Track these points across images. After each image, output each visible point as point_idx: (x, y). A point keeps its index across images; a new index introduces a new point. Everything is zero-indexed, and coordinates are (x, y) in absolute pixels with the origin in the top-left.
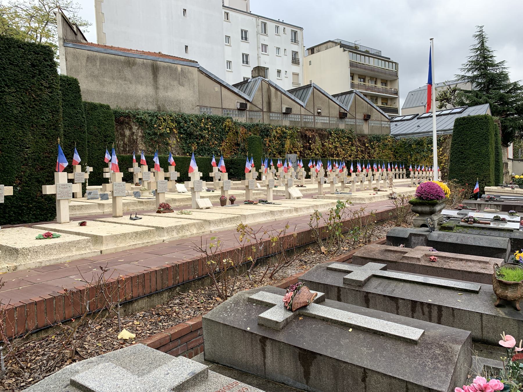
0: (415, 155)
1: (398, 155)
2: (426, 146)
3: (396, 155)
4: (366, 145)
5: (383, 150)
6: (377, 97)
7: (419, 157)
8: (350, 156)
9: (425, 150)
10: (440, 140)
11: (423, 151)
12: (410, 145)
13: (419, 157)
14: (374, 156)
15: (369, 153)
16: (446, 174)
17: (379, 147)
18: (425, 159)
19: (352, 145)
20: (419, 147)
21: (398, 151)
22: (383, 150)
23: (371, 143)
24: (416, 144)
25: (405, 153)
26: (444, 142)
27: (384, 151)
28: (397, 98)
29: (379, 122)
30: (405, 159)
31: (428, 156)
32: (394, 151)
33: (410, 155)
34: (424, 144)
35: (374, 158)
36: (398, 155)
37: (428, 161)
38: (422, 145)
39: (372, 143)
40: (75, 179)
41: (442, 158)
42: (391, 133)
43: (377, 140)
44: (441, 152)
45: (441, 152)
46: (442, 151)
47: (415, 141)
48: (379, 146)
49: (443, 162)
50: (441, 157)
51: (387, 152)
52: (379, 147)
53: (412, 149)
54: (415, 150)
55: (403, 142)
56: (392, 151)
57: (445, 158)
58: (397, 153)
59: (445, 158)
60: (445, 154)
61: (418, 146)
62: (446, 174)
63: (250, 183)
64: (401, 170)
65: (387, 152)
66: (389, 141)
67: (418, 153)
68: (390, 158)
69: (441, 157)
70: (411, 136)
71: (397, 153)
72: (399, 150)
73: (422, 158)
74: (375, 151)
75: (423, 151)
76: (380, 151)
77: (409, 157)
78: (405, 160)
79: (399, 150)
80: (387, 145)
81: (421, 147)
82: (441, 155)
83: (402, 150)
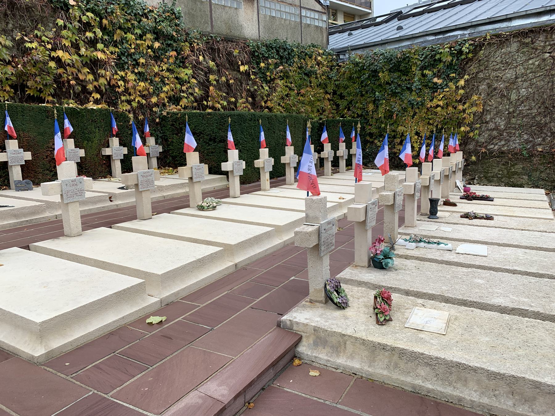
0: (388, 100)
1: (343, 104)
2: (418, 73)
3: (339, 102)
4: (242, 68)
5: (300, 87)
6: (336, 10)
7: (397, 108)
8: (175, 100)
9: (416, 84)
10: (460, 52)
11: (410, 89)
12: (375, 74)
13: (397, 108)
14: (269, 104)
15: (253, 95)
16: (474, 158)
17: (288, 77)
18: (415, 114)
19: (182, 62)
20: (399, 77)
21: (345, 94)
22: (300, 87)
23: (258, 64)
24: (390, 71)
25: (362, 95)
26: (471, 60)
27: (303, 91)
28: (370, 13)
29: (293, 10)
30: (360, 112)
31: (423, 104)
32: (335, 93)
33: (374, 102)
34: (414, 69)
35: (270, 109)
36: (343, 104)
37: (422, 119)
38: (406, 72)
39: (262, 65)
40: (9, 162)
41: (464, 111)
42: (330, 47)
43: (281, 58)
44: (461, 92)
45: (461, 92)
46: (463, 88)
47: (389, 60)
48: (285, 76)
49: (467, 121)
50: (461, 107)
51: (311, 93)
52: (288, 77)
53: (380, 85)
54: (388, 87)
55: (357, 64)
56: (326, 93)
57: (474, 109)
58: (342, 97)
59: (474, 109)
60: (475, 97)
61: (396, 75)
62: (474, 158)
63: (291, 159)
64: (342, 146)
65: (311, 93)
66: (319, 64)
67: (394, 94)
68: (324, 111)
69: (461, 107)
70: (377, 50)
71: (342, 97)
72: (346, 87)
73: (405, 110)
74: (273, 89)
75: (410, 89)
76: (290, 89)
77: (371, 107)
78: (361, 115)
79: (346, 87)
80: (311, 72)
81: (404, 78)
82: (460, 101)
83: (354, 88)
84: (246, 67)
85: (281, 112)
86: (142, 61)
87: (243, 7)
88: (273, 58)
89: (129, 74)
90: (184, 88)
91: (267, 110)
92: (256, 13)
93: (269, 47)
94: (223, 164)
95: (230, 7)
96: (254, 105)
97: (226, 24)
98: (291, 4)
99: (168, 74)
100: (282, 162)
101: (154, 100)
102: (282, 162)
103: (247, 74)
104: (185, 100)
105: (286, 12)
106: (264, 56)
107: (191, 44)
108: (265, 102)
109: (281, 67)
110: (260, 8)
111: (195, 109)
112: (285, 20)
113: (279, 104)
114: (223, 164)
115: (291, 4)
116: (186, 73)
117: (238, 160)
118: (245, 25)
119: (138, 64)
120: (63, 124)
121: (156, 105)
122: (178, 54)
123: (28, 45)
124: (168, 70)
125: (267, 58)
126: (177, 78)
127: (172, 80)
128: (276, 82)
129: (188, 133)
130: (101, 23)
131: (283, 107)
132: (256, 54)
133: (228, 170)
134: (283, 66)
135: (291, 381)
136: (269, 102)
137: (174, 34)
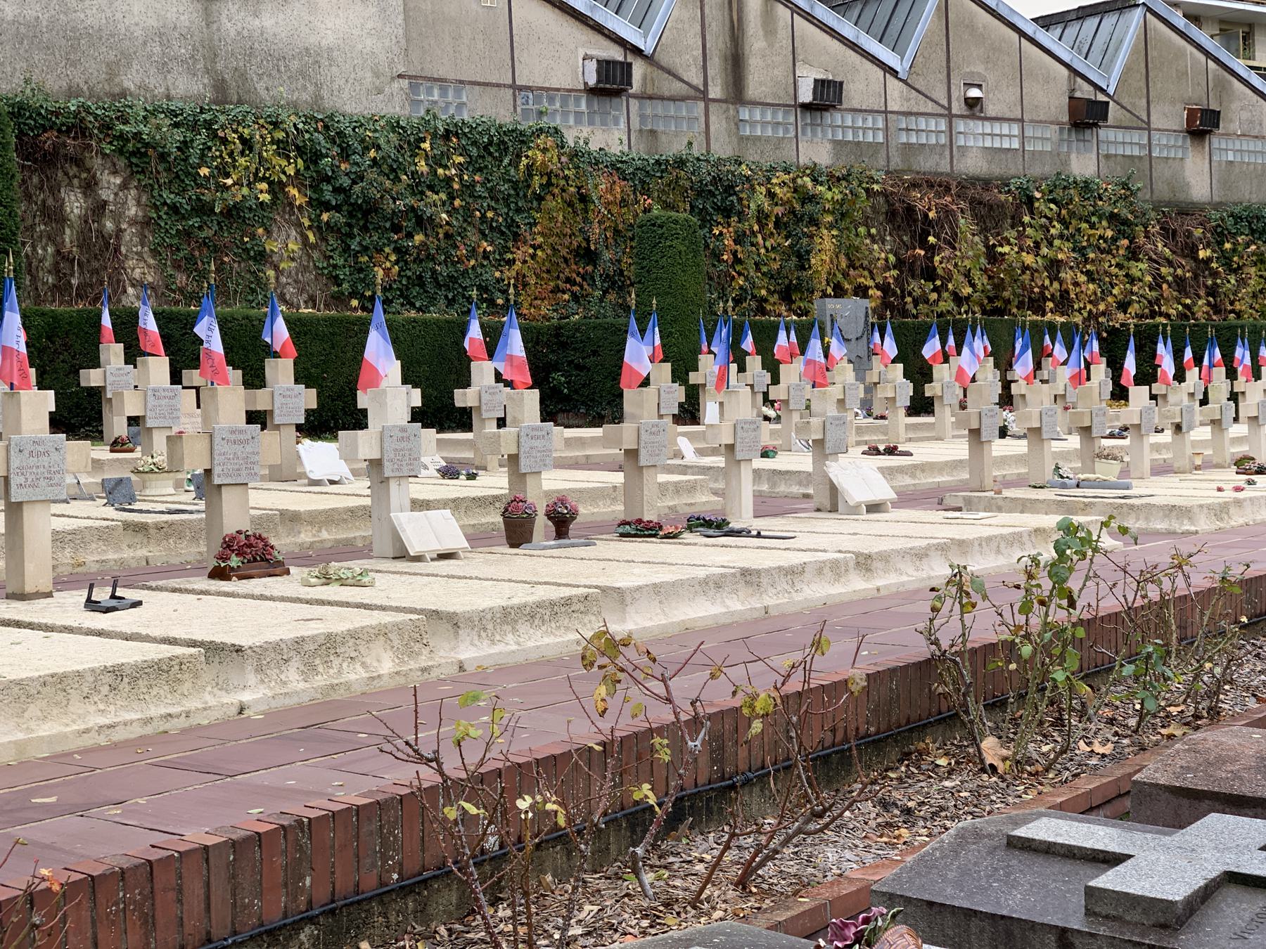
8: (1123, 306)
14: (1238, 306)
15: (1212, 291)
23: (1220, 243)
35: (1239, 315)
39: (1228, 246)
74: (1242, 282)
84: (1208, 253)
85: (1255, 319)
86: (1092, 255)
87: (1191, 155)
88: (1242, 234)
89: (1079, 274)
90: (1135, 289)
91: (1232, 315)
92: (1207, 161)
93: (1237, 218)
94: (458, 393)
95: (1174, 159)
96: (1216, 309)
97: (1169, 184)
98: (1257, 137)
99: (1117, 270)
100: (927, 395)
101: (1102, 307)
102: (927, 395)
103: (1208, 260)
104: (1136, 306)
105: (1249, 152)
106: (1229, 233)
107: (1146, 228)
108: (1232, 303)
109: (1253, 247)
110: (1214, 151)
111: (1147, 318)
112: (1248, 164)
113: (1251, 307)
114: (458, 393)
115: (1257, 137)
116: (1139, 268)
117: (169, 385)
118: (1193, 182)
119: (1086, 261)
120: (1043, 340)
121: (1103, 314)
122: (1131, 242)
123: (999, 249)
124: (1118, 265)
125: (1234, 235)
126: (1127, 275)
127: (1122, 278)
128: (1246, 270)
129: (633, 335)
130: (1059, 215)
131: (1257, 311)
132: (1219, 230)
133: (469, 405)
134: (1255, 244)
135: (308, 881)
136: (1237, 303)
137: (1129, 216)
